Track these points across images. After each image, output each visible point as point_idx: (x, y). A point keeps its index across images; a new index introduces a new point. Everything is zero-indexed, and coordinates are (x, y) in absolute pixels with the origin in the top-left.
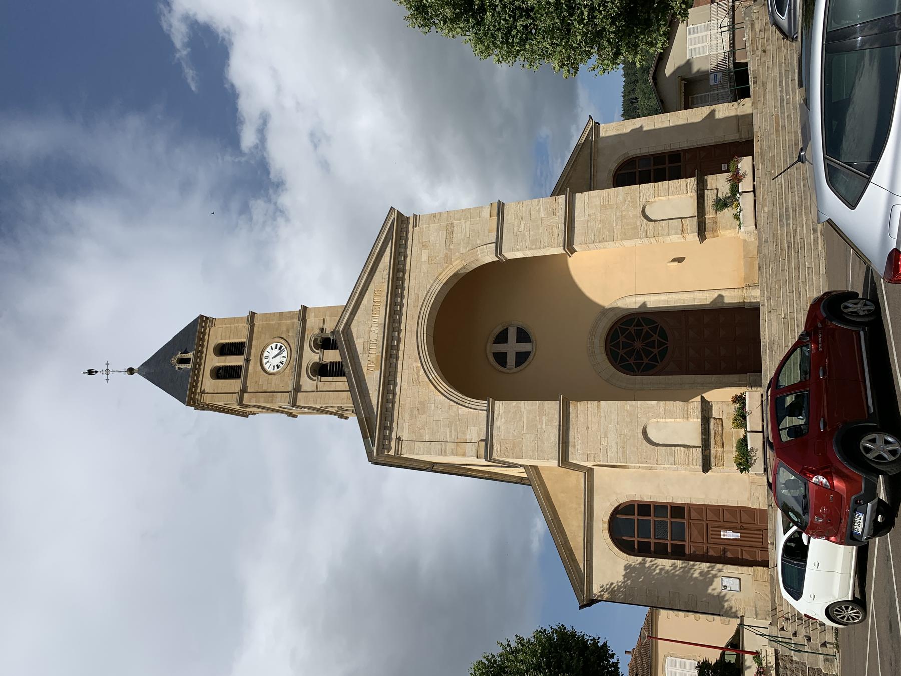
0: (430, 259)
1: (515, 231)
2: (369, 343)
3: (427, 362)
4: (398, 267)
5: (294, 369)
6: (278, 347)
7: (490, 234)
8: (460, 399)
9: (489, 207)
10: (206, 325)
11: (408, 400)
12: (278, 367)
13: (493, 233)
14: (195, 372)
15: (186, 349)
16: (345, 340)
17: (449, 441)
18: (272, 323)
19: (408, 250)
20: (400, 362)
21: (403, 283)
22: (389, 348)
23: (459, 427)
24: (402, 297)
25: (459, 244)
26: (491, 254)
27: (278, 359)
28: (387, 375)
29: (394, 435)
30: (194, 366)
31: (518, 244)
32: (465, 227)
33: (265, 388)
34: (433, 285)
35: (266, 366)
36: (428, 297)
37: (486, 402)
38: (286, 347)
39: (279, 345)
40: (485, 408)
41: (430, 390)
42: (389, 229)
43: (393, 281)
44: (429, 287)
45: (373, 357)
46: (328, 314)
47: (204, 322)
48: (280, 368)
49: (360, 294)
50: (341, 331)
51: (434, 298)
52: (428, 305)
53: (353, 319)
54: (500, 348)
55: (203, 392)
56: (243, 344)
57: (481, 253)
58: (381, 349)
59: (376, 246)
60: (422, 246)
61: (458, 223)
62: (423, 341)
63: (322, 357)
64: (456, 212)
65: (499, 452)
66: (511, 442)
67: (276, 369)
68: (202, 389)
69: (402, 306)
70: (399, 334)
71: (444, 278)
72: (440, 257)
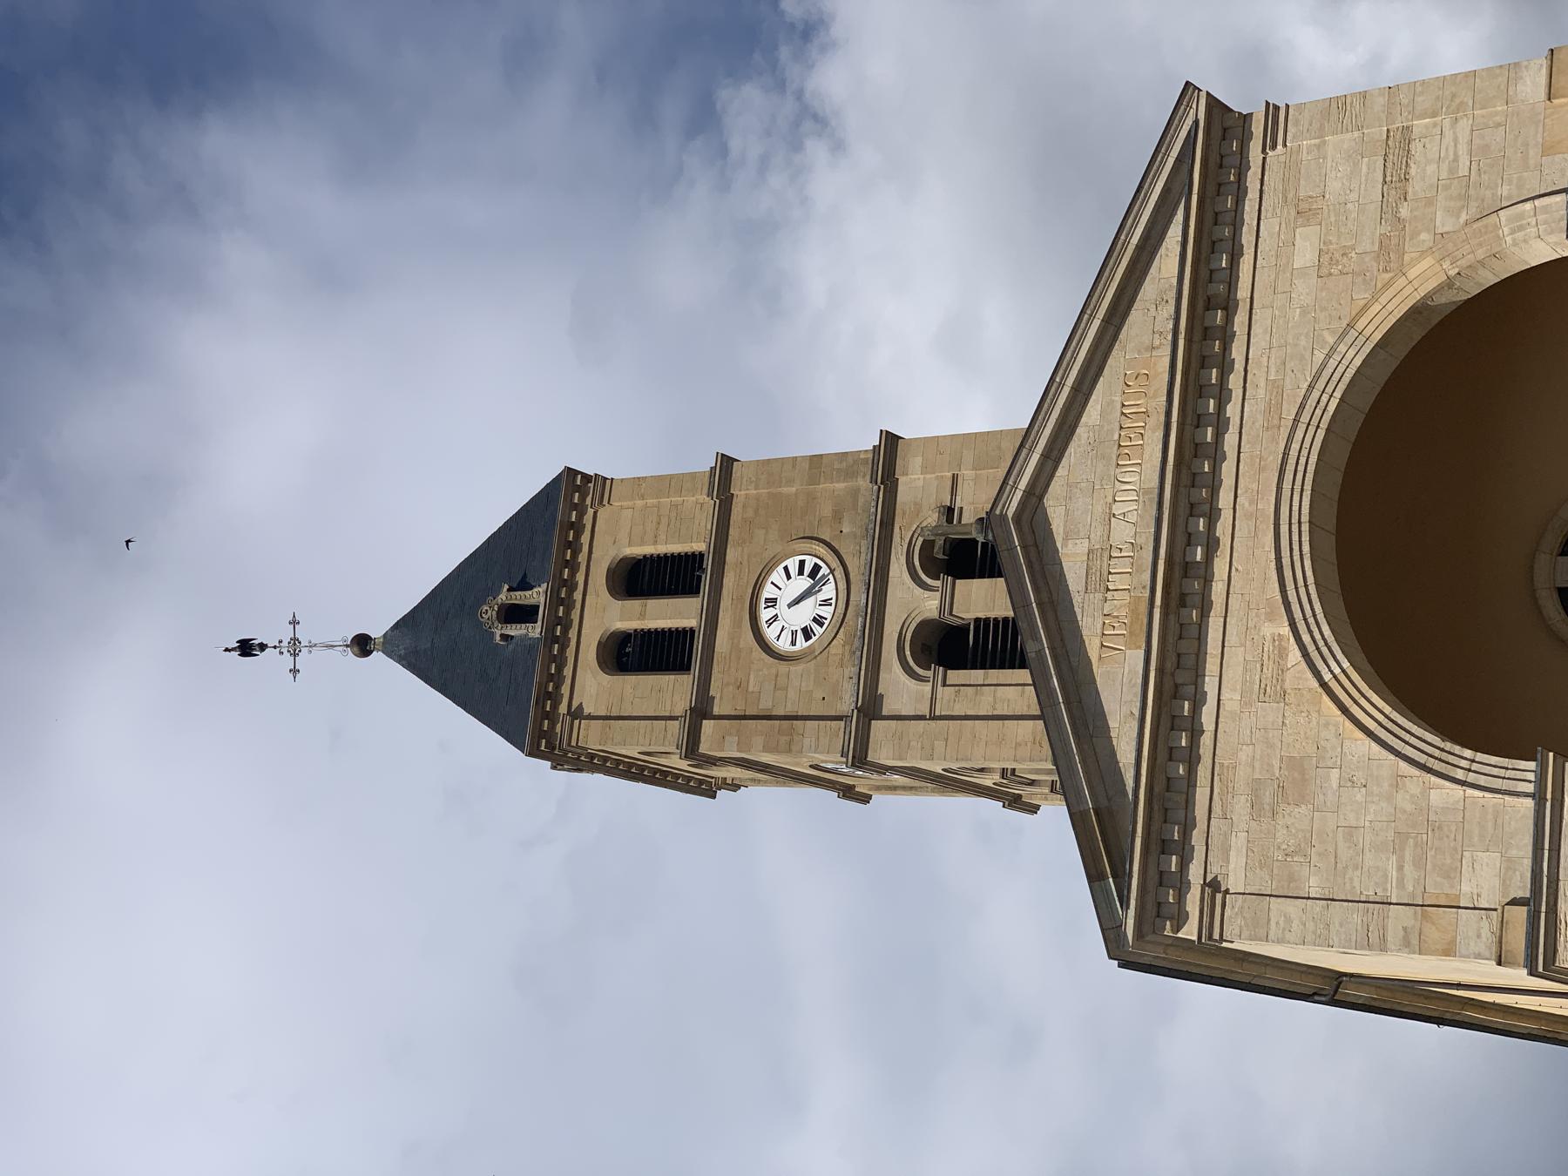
2: (1106, 555)
3: (1311, 620)
5: (857, 643)
6: (807, 570)
8: (1437, 753)
9: (1545, 63)
10: (583, 498)
14: (551, 650)
15: (525, 576)
17: (1394, 901)
18: (785, 490)
21: (1226, 348)
24: (1223, 396)
25: (1430, 202)
26: (1552, 232)
27: (808, 609)
29: (1195, 873)
33: (765, 705)
34: (1333, 350)
35: (770, 633)
36: (1316, 394)
37: (1532, 765)
38: (832, 571)
39: (810, 562)
40: (1530, 788)
41: (1322, 722)
42: (1178, 160)
44: (1319, 356)
45: (1120, 604)
46: (968, 457)
48: (814, 639)
49: (1076, 389)
50: (1010, 514)
51: (1338, 394)
52: (1315, 422)
55: (577, 714)
57: (1513, 232)
58: (1147, 576)
60: (1293, 213)
61: (1426, 127)
63: (948, 603)
64: (1419, 89)
67: (801, 643)
68: (575, 704)
69: (1221, 425)
70: (1211, 526)
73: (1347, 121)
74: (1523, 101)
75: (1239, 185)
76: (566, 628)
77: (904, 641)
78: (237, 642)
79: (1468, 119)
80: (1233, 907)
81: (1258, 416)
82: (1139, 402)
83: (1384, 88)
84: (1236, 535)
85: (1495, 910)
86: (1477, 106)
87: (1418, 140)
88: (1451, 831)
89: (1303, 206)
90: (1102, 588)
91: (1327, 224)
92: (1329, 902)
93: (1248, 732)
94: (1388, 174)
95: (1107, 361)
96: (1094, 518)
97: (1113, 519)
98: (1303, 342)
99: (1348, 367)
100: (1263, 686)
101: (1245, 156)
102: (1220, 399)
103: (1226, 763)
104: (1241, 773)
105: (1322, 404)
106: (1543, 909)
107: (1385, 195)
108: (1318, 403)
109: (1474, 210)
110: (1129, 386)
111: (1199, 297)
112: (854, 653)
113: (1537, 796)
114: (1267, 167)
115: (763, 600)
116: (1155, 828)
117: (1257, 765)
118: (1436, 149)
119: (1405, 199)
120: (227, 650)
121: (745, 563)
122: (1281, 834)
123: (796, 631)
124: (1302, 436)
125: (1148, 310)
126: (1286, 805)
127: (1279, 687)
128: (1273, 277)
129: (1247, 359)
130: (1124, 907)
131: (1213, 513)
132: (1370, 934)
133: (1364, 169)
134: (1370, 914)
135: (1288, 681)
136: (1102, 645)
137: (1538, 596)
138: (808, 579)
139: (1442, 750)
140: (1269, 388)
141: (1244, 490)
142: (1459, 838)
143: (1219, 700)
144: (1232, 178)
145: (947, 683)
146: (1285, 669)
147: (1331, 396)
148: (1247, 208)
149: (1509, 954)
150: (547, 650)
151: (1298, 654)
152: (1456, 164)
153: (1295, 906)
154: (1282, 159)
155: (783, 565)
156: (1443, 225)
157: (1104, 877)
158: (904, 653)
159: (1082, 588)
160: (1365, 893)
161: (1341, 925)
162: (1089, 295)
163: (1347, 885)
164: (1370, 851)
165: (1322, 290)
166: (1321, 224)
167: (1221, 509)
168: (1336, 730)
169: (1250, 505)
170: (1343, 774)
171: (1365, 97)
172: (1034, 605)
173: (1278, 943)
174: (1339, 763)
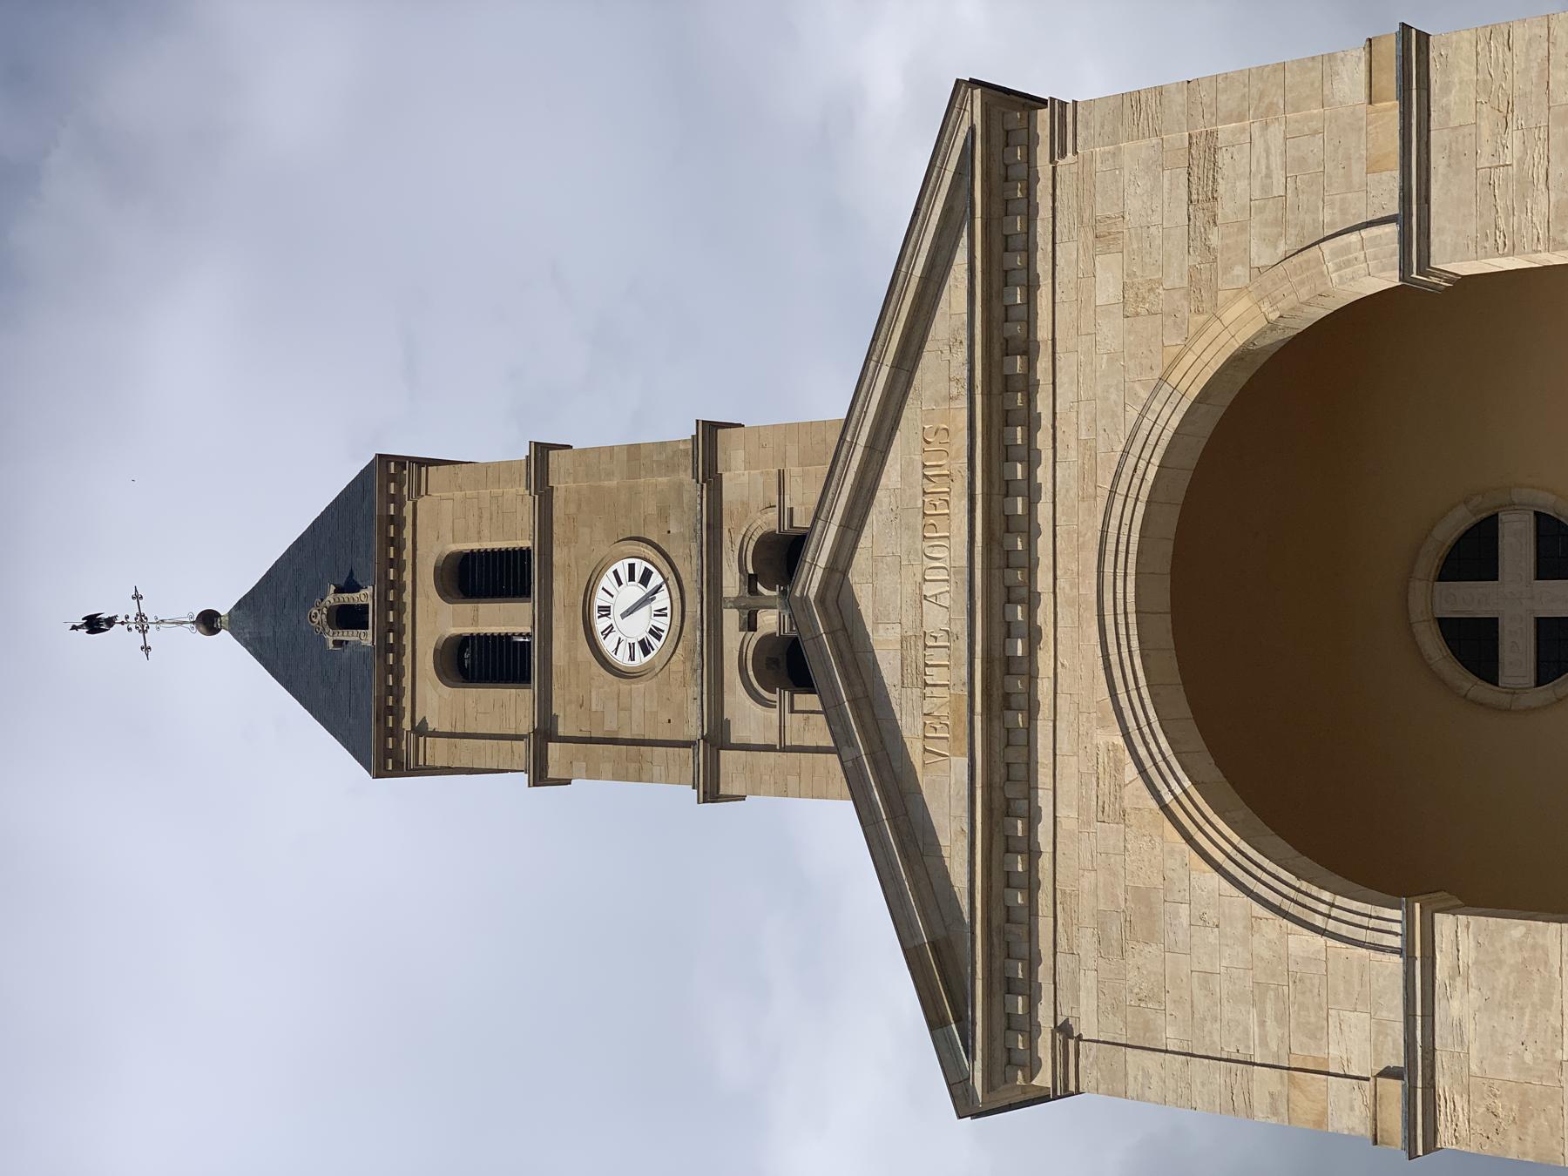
0: (1130, 294)
1: (1484, 162)
2: (920, 644)
3: (1146, 730)
4: (1007, 335)
5: (697, 660)
6: (638, 574)
7: (1376, 176)
8: (1292, 894)
9: (1364, 55)
11: (1088, 880)
12: (646, 652)
13: (1385, 176)
14: (386, 660)
15: (351, 573)
16: (831, 633)
19: (1039, 254)
21: (1030, 400)
22: (998, 672)
24: (1032, 461)
25: (1243, 228)
26: (1384, 270)
28: (997, 779)
30: (381, 639)
31: (1502, 223)
33: (610, 727)
34: (1146, 408)
35: (608, 645)
36: (1131, 461)
37: (1397, 914)
39: (640, 566)
40: (1396, 942)
43: (987, 394)
44: (1133, 414)
46: (793, 451)
47: (392, 478)
48: (653, 653)
49: (871, 446)
50: (812, 596)
51: (1156, 461)
54: (1468, 599)
55: (421, 730)
56: (524, 554)
57: (1339, 268)
58: (964, 672)
60: (1091, 237)
62: (1123, 642)
64: (1222, 85)
66: (1511, 1090)
67: (640, 659)
68: (418, 720)
70: (1031, 614)
71: (1191, 375)
73: (1143, 123)
74: (1341, 103)
75: (1029, 202)
76: (399, 635)
77: (746, 659)
78: (83, 619)
79: (1280, 124)
80: (1087, 1057)
81: (1072, 483)
82: (940, 463)
83: (1183, 82)
84: (1059, 625)
85: (1367, 1079)
86: (1288, 108)
87: (1224, 149)
88: (1313, 985)
89: (1101, 229)
91: (1129, 251)
92: (1189, 1058)
93: (1089, 855)
94: (1194, 192)
96: (904, 600)
97: (924, 602)
99: (1164, 428)
100: (1100, 803)
101: (1032, 165)
102: (1029, 461)
104: (1084, 901)
105: (1140, 472)
106: (1419, 1084)
107: (1191, 217)
109: (1293, 243)
110: (928, 443)
112: (695, 670)
113: (1404, 953)
114: (1058, 178)
116: (997, 964)
117: (1101, 893)
118: (1246, 160)
119: (1215, 223)
120: (74, 628)
121: (573, 565)
122: (1132, 975)
123: (634, 644)
124: (1121, 510)
125: (942, 352)
126: (1135, 943)
127: (1117, 806)
128: (1074, 315)
129: (1054, 413)
130: (970, 1056)
131: (1032, 597)
134: (1233, 1074)
136: (925, 750)
137: (1414, 630)
138: (640, 585)
139: (1298, 890)
140: (1081, 449)
143: (1055, 817)
145: (796, 708)
146: (1122, 786)
147: (1149, 463)
148: (1039, 229)
149: (1385, 1134)
150: (382, 660)
151: (1135, 770)
152: (1269, 181)
153: (1152, 1059)
154: (1074, 169)
156: (1259, 258)
157: (948, 1024)
158: (747, 672)
159: (897, 681)
160: (1226, 1049)
161: (1203, 1084)
162: (873, 339)
163: (1207, 1039)
164: (1229, 1001)
165: (1129, 333)
166: (1122, 252)
168: (1183, 860)
169: (1071, 589)
171: (1161, 94)
172: (846, 704)
173: (1138, 1099)
174: (1187, 898)
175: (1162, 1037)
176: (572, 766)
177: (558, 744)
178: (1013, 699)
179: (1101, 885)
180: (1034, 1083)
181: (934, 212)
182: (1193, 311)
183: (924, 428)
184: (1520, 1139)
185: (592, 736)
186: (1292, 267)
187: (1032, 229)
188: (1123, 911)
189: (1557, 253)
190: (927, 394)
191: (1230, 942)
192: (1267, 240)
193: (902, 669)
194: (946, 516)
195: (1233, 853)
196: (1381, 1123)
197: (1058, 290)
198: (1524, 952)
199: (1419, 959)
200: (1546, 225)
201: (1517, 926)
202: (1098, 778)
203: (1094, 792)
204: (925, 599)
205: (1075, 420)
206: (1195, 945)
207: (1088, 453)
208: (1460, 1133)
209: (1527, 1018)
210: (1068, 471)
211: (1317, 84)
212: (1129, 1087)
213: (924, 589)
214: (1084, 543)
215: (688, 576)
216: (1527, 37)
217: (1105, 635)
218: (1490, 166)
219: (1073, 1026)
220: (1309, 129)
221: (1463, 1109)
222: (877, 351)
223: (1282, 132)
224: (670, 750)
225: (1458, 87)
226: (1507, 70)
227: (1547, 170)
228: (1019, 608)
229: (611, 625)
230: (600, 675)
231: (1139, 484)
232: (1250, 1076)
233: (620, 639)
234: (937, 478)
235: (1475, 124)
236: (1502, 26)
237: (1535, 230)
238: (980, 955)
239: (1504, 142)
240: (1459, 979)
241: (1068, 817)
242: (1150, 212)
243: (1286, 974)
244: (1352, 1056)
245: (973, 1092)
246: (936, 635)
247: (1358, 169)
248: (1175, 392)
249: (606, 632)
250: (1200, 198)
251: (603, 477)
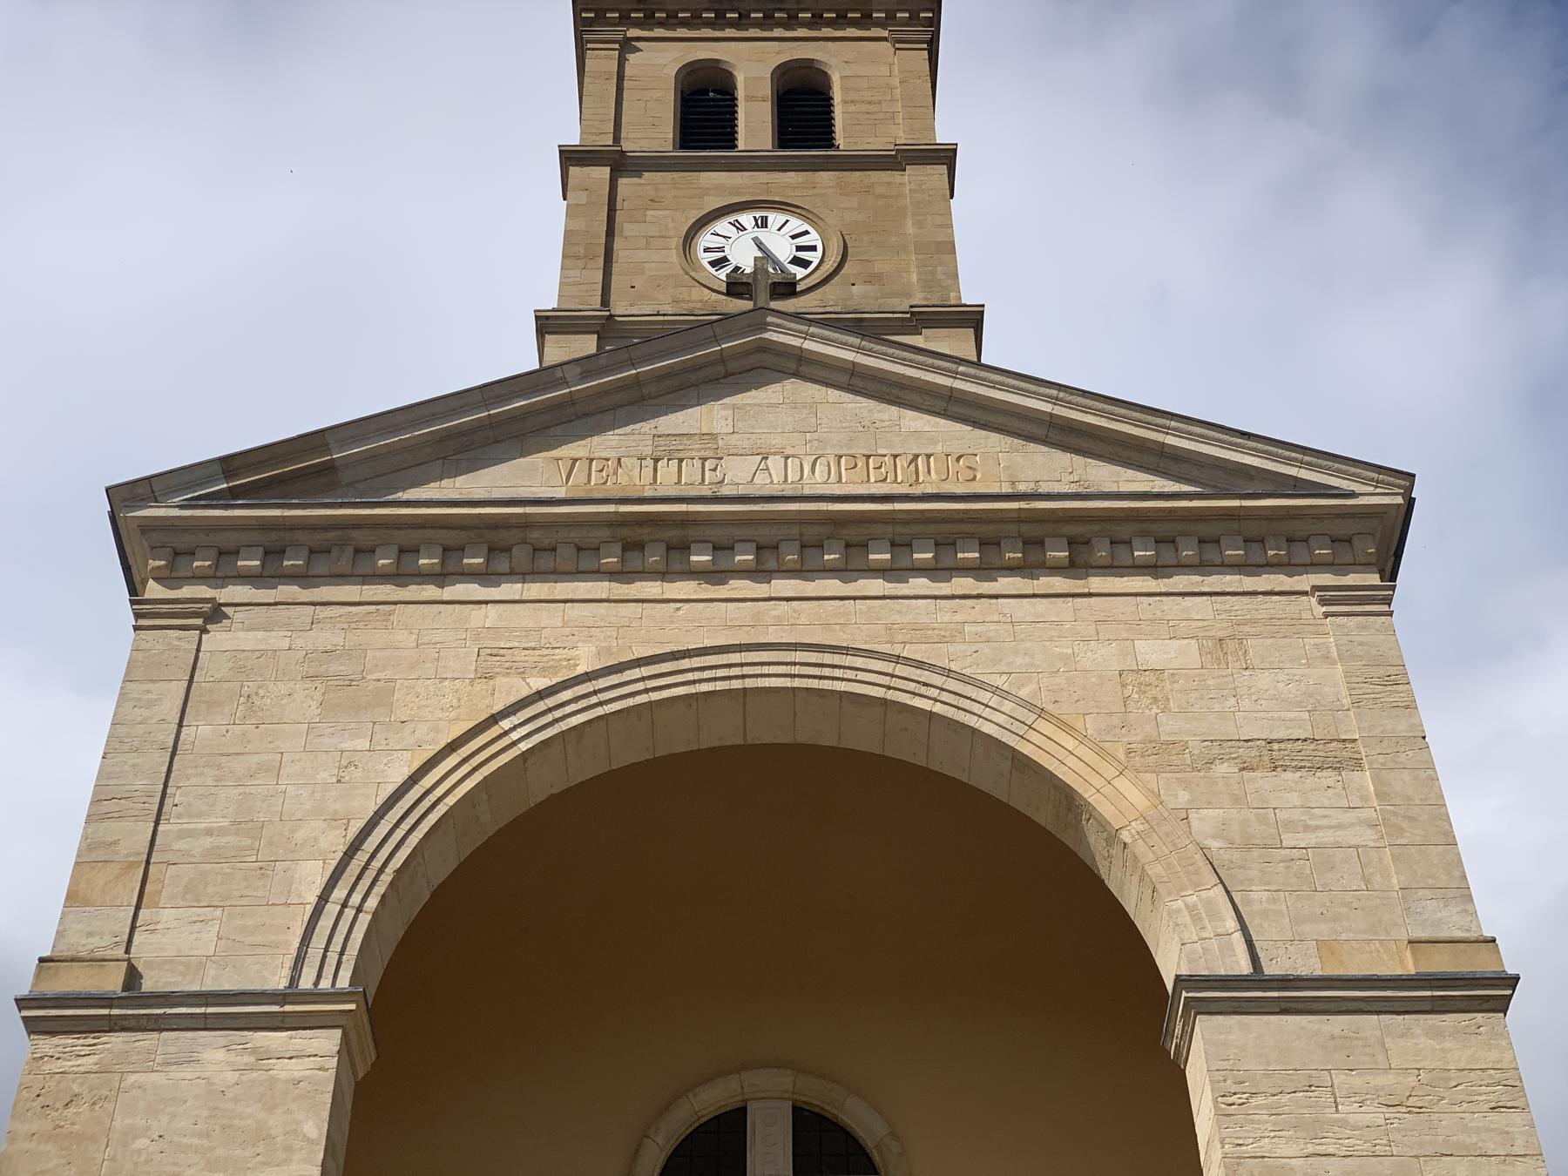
0: (1149, 678)
1: (1339, 1078)
3: (594, 700)
8: (377, 864)
11: (404, 638)
12: (713, 264)
16: (722, 358)
17: (161, 828)
20: (601, 588)
22: (673, 534)
23: (226, 868)
24: (934, 571)
25: (1237, 800)
28: (535, 535)
32: (1339, 827)
34: (1004, 694)
35: (723, 226)
36: (937, 680)
37: (344, 982)
40: (306, 983)
44: (999, 681)
48: (712, 270)
50: (767, 335)
51: (938, 708)
53: (828, 385)
55: (627, 46)
57: (1191, 909)
59: (1198, 430)
60: (1221, 634)
62: (707, 674)
64: (1422, 775)
65: (55, 1066)
67: (705, 259)
72: (1162, 718)
75: (1262, 566)
82: (933, 472)
84: (729, 604)
85: (127, 951)
86: (1397, 850)
87: (1340, 778)
89: (1231, 646)
90: (659, 454)
91: (1204, 675)
92: (171, 750)
94: (1283, 746)
95: (992, 431)
97: (760, 457)
98: (1019, 661)
99: (980, 716)
100: (502, 652)
103: (394, 618)
105: (923, 690)
107: (1250, 743)
108: (925, 684)
109: (1222, 857)
110: (958, 459)
111: (1087, 526)
114: (1293, 598)
115: (764, 214)
116: (301, 536)
117: (387, 653)
119: (1244, 769)
121: (815, 191)
122: (283, 688)
123: (724, 251)
125: (1070, 473)
131: (765, 574)
132: (117, 800)
133: (1289, 715)
134: (146, 799)
135: (507, 679)
136: (575, 460)
139: (381, 871)
141: (797, 607)
142: (244, 901)
143: (486, 602)
144: (1271, 553)
146: (523, 676)
149: (53, 971)
155: (810, 229)
156: (1200, 819)
159: (661, 430)
161: (134, 766)
162: (1084, 392)
163: (193, 771)
166: (1202, 668)
167: (770, 582)
169: (775, 617)
170: (360, 754)
171: (1407, 707)
172: (634, 372)
175: (199, 721)
176: (582, 190)
177: (608, 176)
178: (637, 553)
179: (398, 653)
180: (151, 582)
181: (1246, 456)
182: (1129, 746)
183: (976, 455)
184: (34, 1134)
185: (617, 212)
186: (1190, 855)
187: (1229, 569)
188: (363, 678)
189: (1222, 1168)
190: (1018, 457)
191: (318, 796)
192: (1223, 827)
193: (676, 435)
194: (866, 479)
195: (432, 798)
196: (67, 966)
197: (1151, 599)
198: (282, 1137)
199: (281, 1009)
200: (1258, 1154)
201: (319, 1128)
202: (534, 649)
203: (516, 644)
204: (763, 458)
205: (988, 619)
206: (316, 756)
207: (947, 634)
208: (46, 1062)
209: (196, 1141)
210: (925, 613)
211: (1430, 881)
212: (137, 684)
213: (776, 457)
214: (833, 630)
215: (802, 304)
216: (1509, 1129)
217: (716, 654)
218: (1335, 1086)
219: (219, 625)
220: (1371, 874)
221: (79, 1065)
222: (1071, 398)
223: (1365, 843)
224: (600, 286)
225: (1438, 1047)
226: (1465, 1105)
227: (1334, 1155)
228: (751, 557)
229: (745, 229)
230: (687, 219)
231: (908, 689)
232: (140, 818)
233: (730, 238)
234: (914, 469)
235: (1390, 1068)
236: (1523, 1099)
237: (1251, 1141)
238: (313, 514)
239: (1368, 1102)
240: (252, 1059)
241: (486, 616)
242: (1254, 698)
243: (272, 859)
244: (159, 936)
245: (140, 506)
246: (718, 470)
247: (1323, 930)
248: (1027, 728)
249: (737, 224)
250: (1274, 753)
251: (915, 217)
